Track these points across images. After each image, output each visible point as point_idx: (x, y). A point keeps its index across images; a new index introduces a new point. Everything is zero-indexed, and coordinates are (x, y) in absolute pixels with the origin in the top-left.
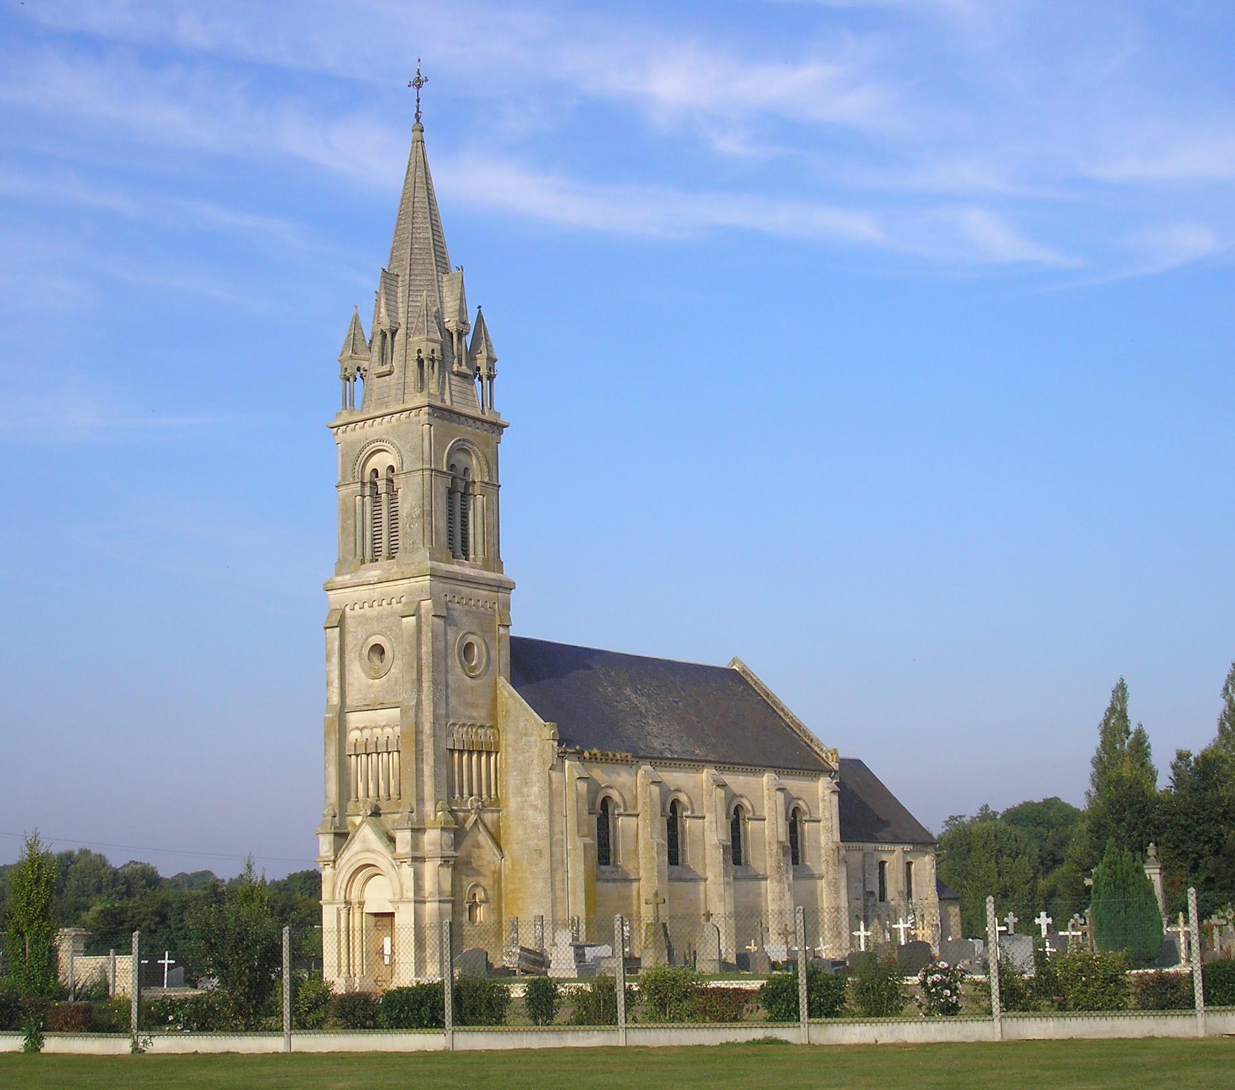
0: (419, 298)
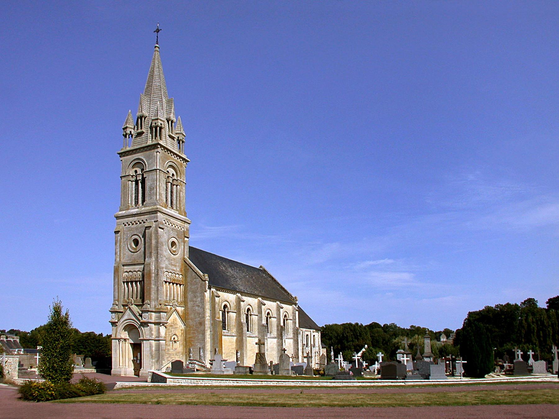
0: (156, 106)
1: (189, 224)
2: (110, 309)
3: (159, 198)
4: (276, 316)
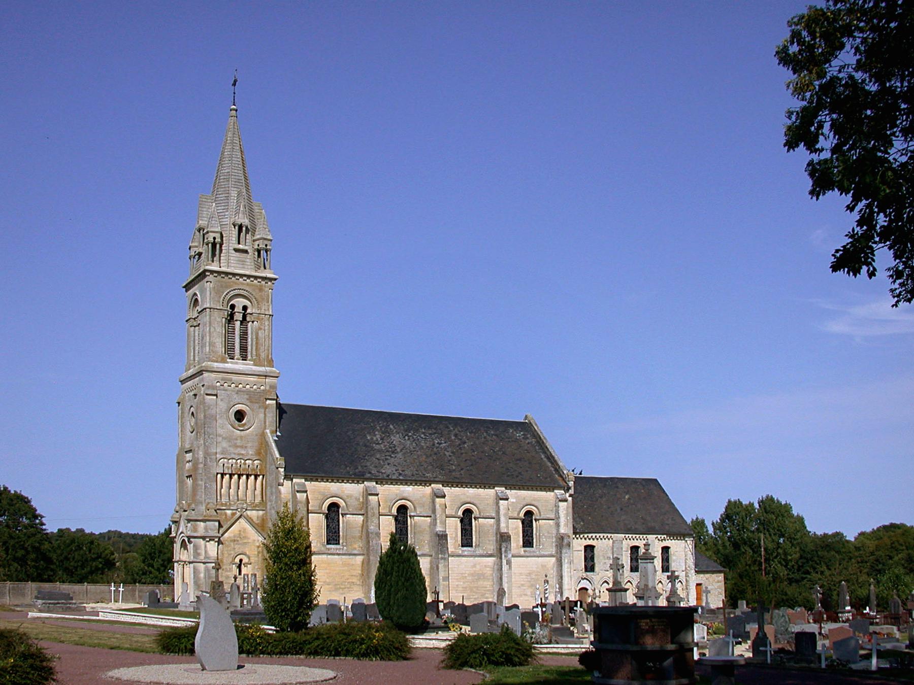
1: (277, 377)
2: (170, 519)
3: (210, 349)
4: (494, 515)
